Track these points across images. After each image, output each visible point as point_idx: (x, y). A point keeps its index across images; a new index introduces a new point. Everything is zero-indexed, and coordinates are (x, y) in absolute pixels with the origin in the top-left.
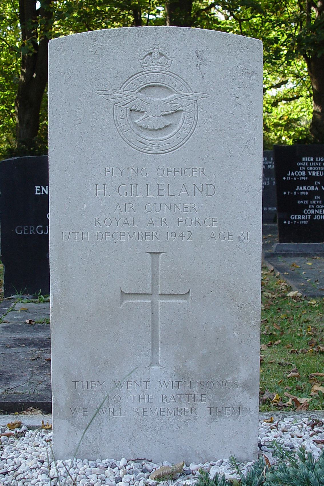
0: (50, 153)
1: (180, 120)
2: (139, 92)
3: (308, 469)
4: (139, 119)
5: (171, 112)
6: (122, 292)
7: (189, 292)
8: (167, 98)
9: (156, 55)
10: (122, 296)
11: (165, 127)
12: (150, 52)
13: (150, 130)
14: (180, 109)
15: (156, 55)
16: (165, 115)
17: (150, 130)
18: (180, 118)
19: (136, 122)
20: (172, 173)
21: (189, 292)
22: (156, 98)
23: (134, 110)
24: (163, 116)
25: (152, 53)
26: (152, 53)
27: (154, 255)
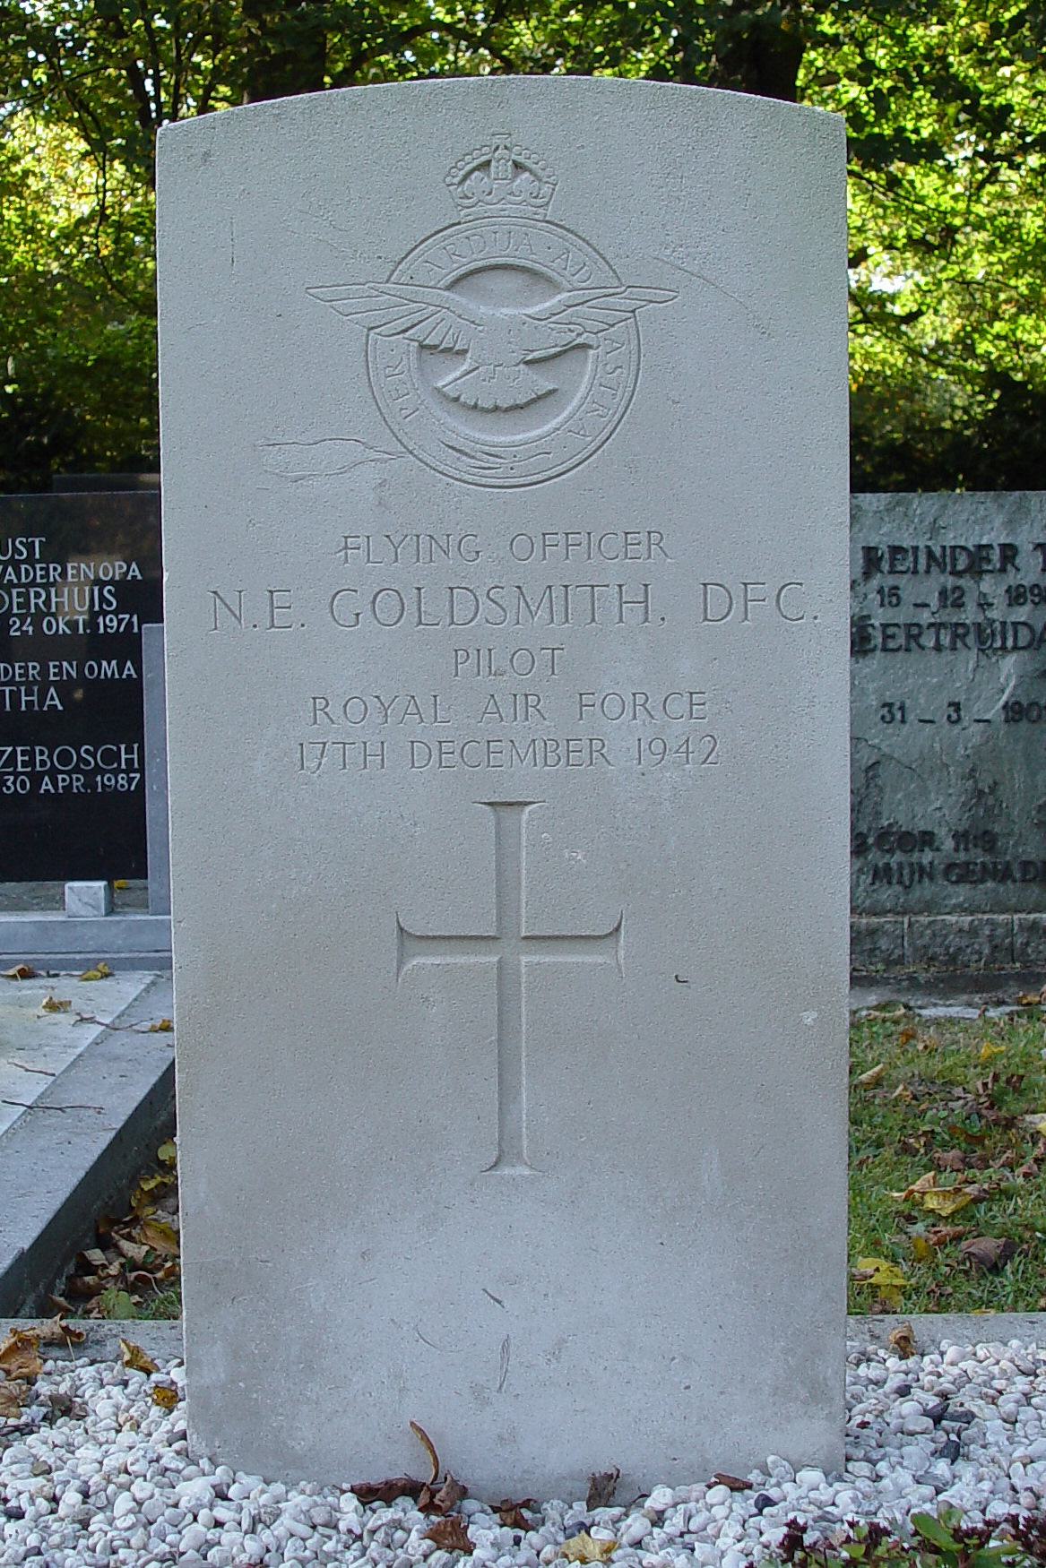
0: (167, 464)
1: (583, 378)
2: (448, 288)
3: (68, 209)
4: (449, 377)
5: (553, 351)
6: (402, 929)
7: (617, 929)
8: (537, 309)
9: (500, 168)
10: (402, 944)
11: (533, 401)
12: (483, 159)
13: (507, 410)
14: (580, 340)
15: (500, 168)
16: (527, 363)
17: (464, 405)
18: (582, 375)
19: (440, 384)
20: (561, 549)
21: (617, 929)
22: (506, 311)
23: (436, 347)
24: (527, 363)
25: (489, 162)
26: (489, 162)
27: (505, 813)
